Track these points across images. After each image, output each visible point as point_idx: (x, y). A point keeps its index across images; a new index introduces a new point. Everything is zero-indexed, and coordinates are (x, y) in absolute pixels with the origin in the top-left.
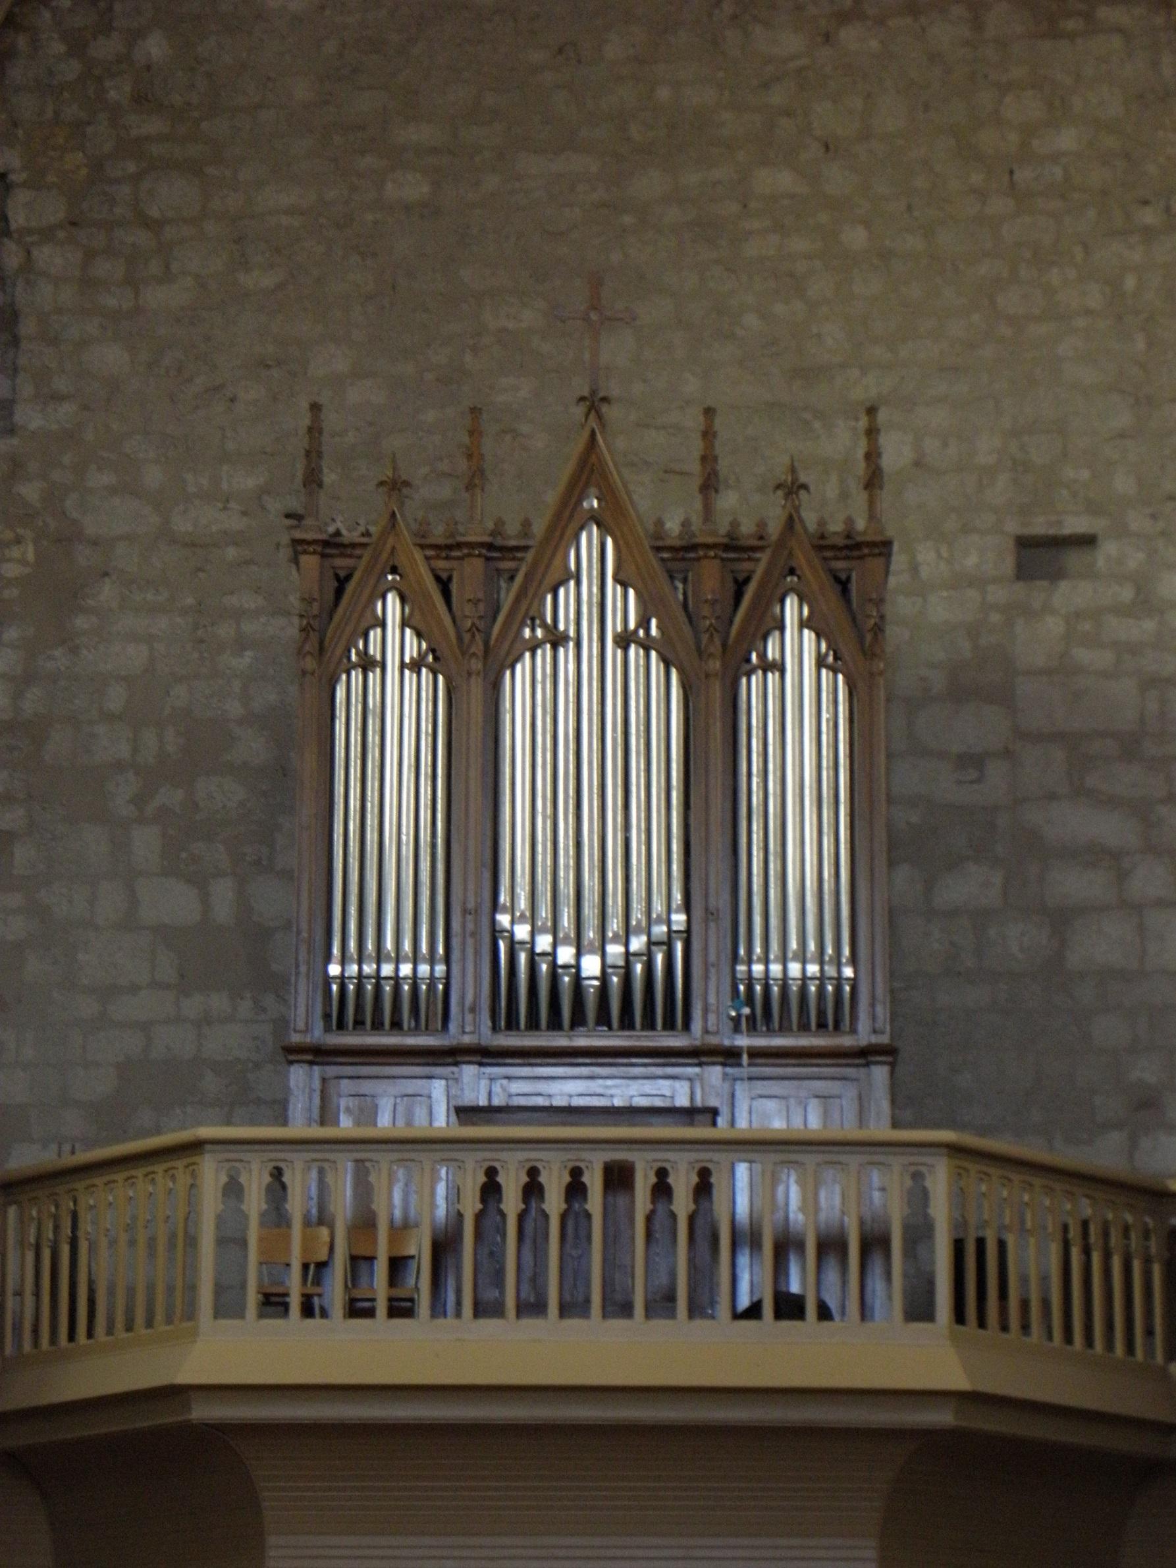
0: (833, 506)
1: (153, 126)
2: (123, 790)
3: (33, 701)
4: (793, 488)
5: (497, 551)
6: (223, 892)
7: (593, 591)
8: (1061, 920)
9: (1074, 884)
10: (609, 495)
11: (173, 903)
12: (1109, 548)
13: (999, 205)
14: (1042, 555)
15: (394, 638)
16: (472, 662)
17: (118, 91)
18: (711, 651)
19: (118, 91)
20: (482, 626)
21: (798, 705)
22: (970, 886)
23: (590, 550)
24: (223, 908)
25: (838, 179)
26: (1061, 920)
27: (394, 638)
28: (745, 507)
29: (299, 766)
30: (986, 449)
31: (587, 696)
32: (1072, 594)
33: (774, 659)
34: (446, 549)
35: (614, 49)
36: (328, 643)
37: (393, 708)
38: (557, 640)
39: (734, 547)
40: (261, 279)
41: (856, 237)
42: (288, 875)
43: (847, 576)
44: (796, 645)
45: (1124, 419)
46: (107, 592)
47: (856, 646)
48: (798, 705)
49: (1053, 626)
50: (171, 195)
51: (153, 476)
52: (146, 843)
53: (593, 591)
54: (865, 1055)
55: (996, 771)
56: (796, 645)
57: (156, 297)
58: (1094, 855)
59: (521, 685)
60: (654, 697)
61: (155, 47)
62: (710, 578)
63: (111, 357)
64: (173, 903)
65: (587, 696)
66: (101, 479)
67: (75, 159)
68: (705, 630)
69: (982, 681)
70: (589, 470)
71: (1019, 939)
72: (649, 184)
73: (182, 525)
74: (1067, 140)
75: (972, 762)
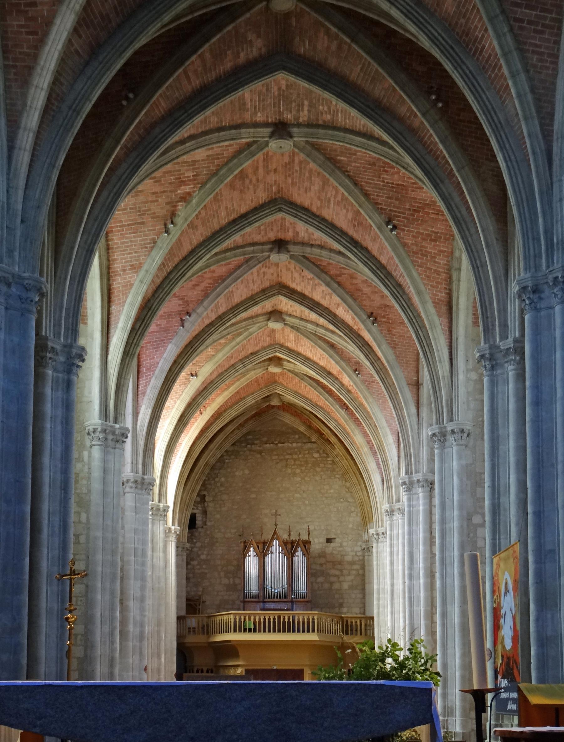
0: (305, 537)
1: (222, 489)
2: (220, 568)
3: (209, 557)
4: (299, 535)
5: (264, 543)
6: (231, 580)
7: (276, 547)
8: (331, 583)
9: (333, 579)
10: (277, 535)
11: (226, 581)
12: (337, 540)
13: (324, 499)
14: (329, 541)
15: (252, 552)
16: (262, 556)
17: (219, 485)
18: (290, 556)
19: (219, 485)
20: (263, 551)
21: (300, 560)
22: (321, 579)
23: (275, 542)
24: (231, 582)
25: (305, 495)
26: (331, 583)
27: (252, 552)
28: (294, 537)
29: (241, 568)
30: (323, 528)
31: (275, 560)
32: (332, 545)
33: (359, 130)
34: (259, 542)
35: (278, 480)
36: (245, 553)
37: (252, 563)
38: (271, 553)
39: (292, 542)
40: (236, 507)
41: (307, 502)
42: (240, 578)
43: (306, 544)
44: (300, 553)
45: (339, 524)
46: (217, 544)
47: (307, 553)
48: (300, 560)
49: (331, 548)
50: (225, 497)
51: (223, 530)
52: (222, 574)
53: (276, 547)
54: (307, 602)
55: (324, 566)
56: (300, 553)
57: (224, 509)
58: (336, 576)
59: (267, 559)
60: (284, 560)
61: (223, 479)
62: (289, 546)
63: (218, 516)
64: (226, 581)
65: (275, 560)
66: (216, 531)
67: (213, 493)
68: (290, 549)
69: (322, 555)
70: (275, 533)
71: (326, 586)
72: (282, 496)
73: (226, 536)
74: (332, 491)
75: (321, 565)
